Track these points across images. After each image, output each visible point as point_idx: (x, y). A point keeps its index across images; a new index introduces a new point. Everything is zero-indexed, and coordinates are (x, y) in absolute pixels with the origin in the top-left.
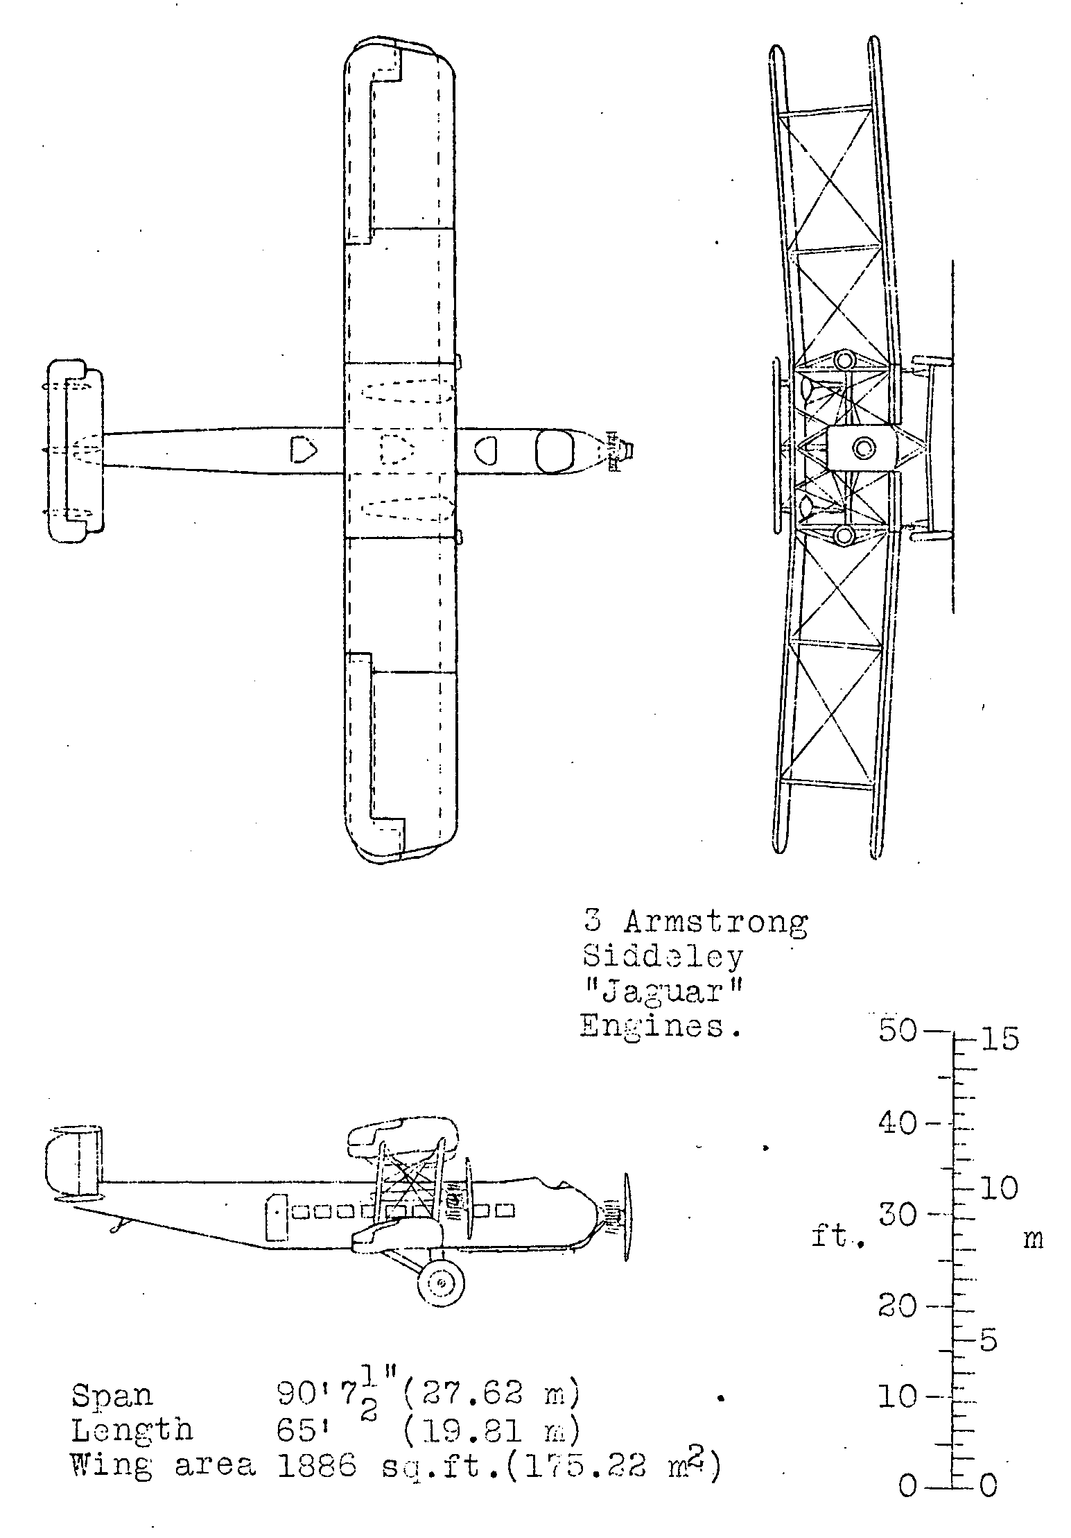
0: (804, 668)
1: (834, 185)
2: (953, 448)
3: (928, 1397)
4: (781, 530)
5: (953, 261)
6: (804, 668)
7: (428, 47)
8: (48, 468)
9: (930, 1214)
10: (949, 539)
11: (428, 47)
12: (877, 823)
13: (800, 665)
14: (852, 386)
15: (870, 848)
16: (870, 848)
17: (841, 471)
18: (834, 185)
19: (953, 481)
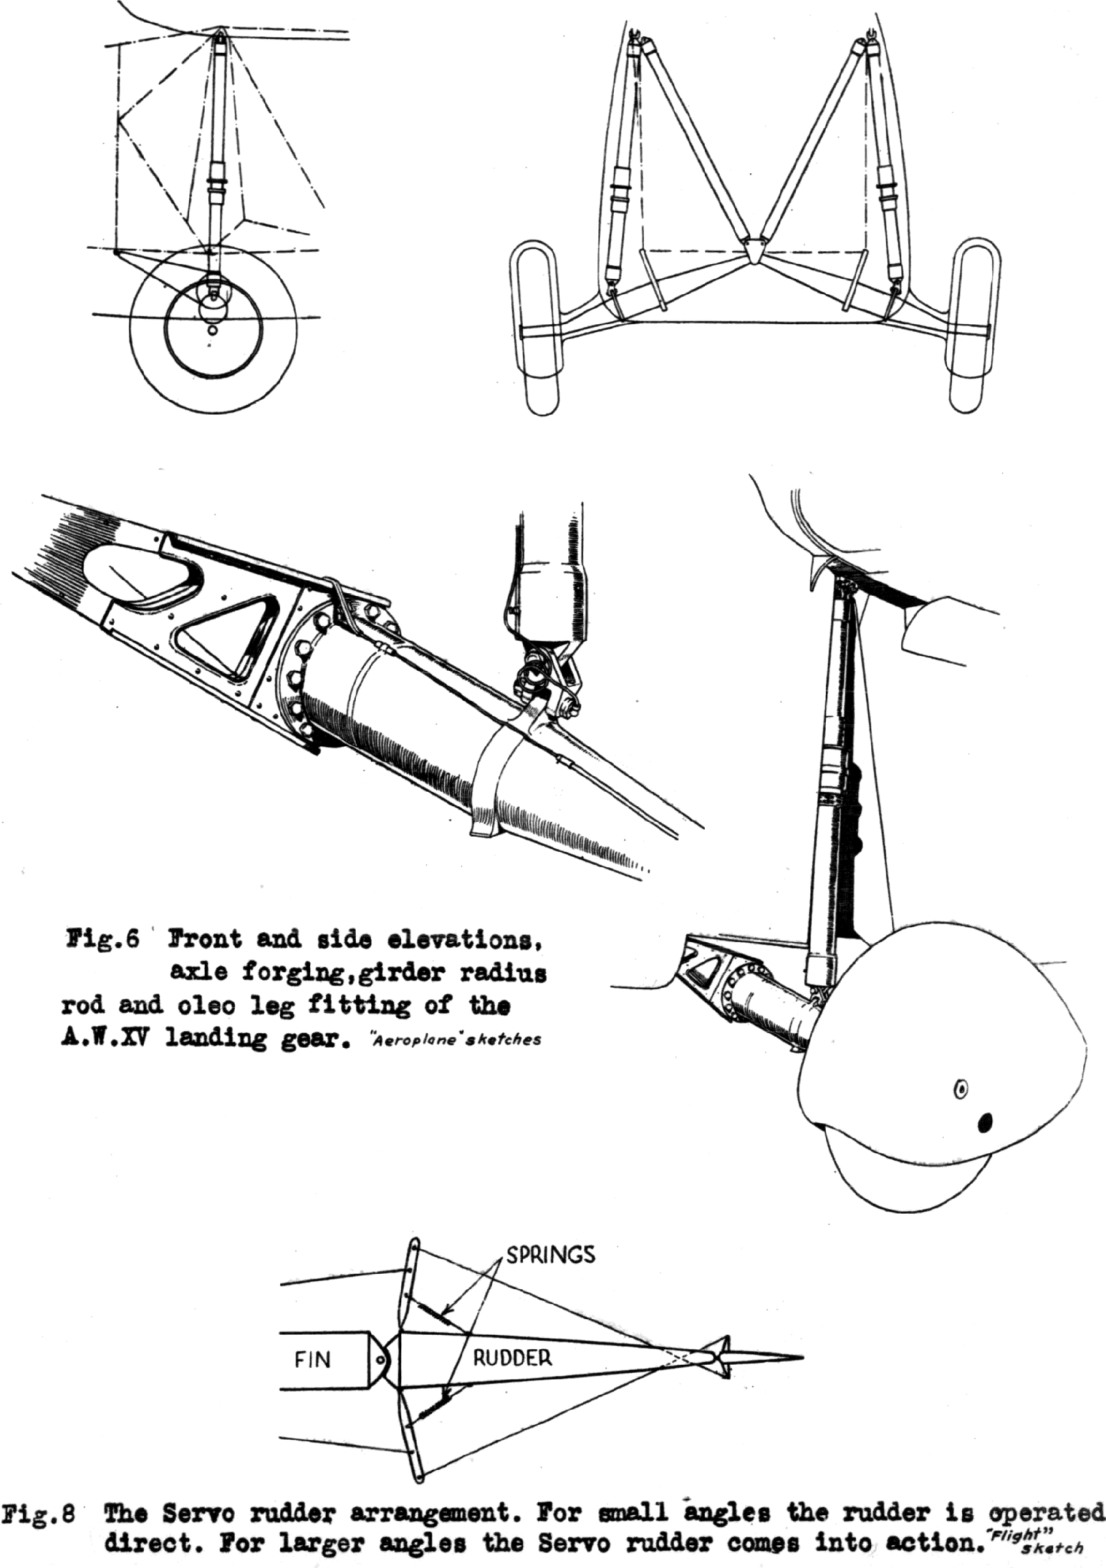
0: (905, 618)
1: (399, 1451)
2: (675, 113)
3: (14, 574)
4: (957, 259)
5: (319, 318)
6: (905, 618)
7: (990, 370)
8: (1077, 1026)
9: (582, 504)
10: (222, 307)
11: (990, 370)
12: (724, 973)
13: (908, 622)
14: (411, 1425)
15: (671, 1362)
16: (671, 1362)
17: (684, 952)
18: (399, 1451)
19: (282, 281)
